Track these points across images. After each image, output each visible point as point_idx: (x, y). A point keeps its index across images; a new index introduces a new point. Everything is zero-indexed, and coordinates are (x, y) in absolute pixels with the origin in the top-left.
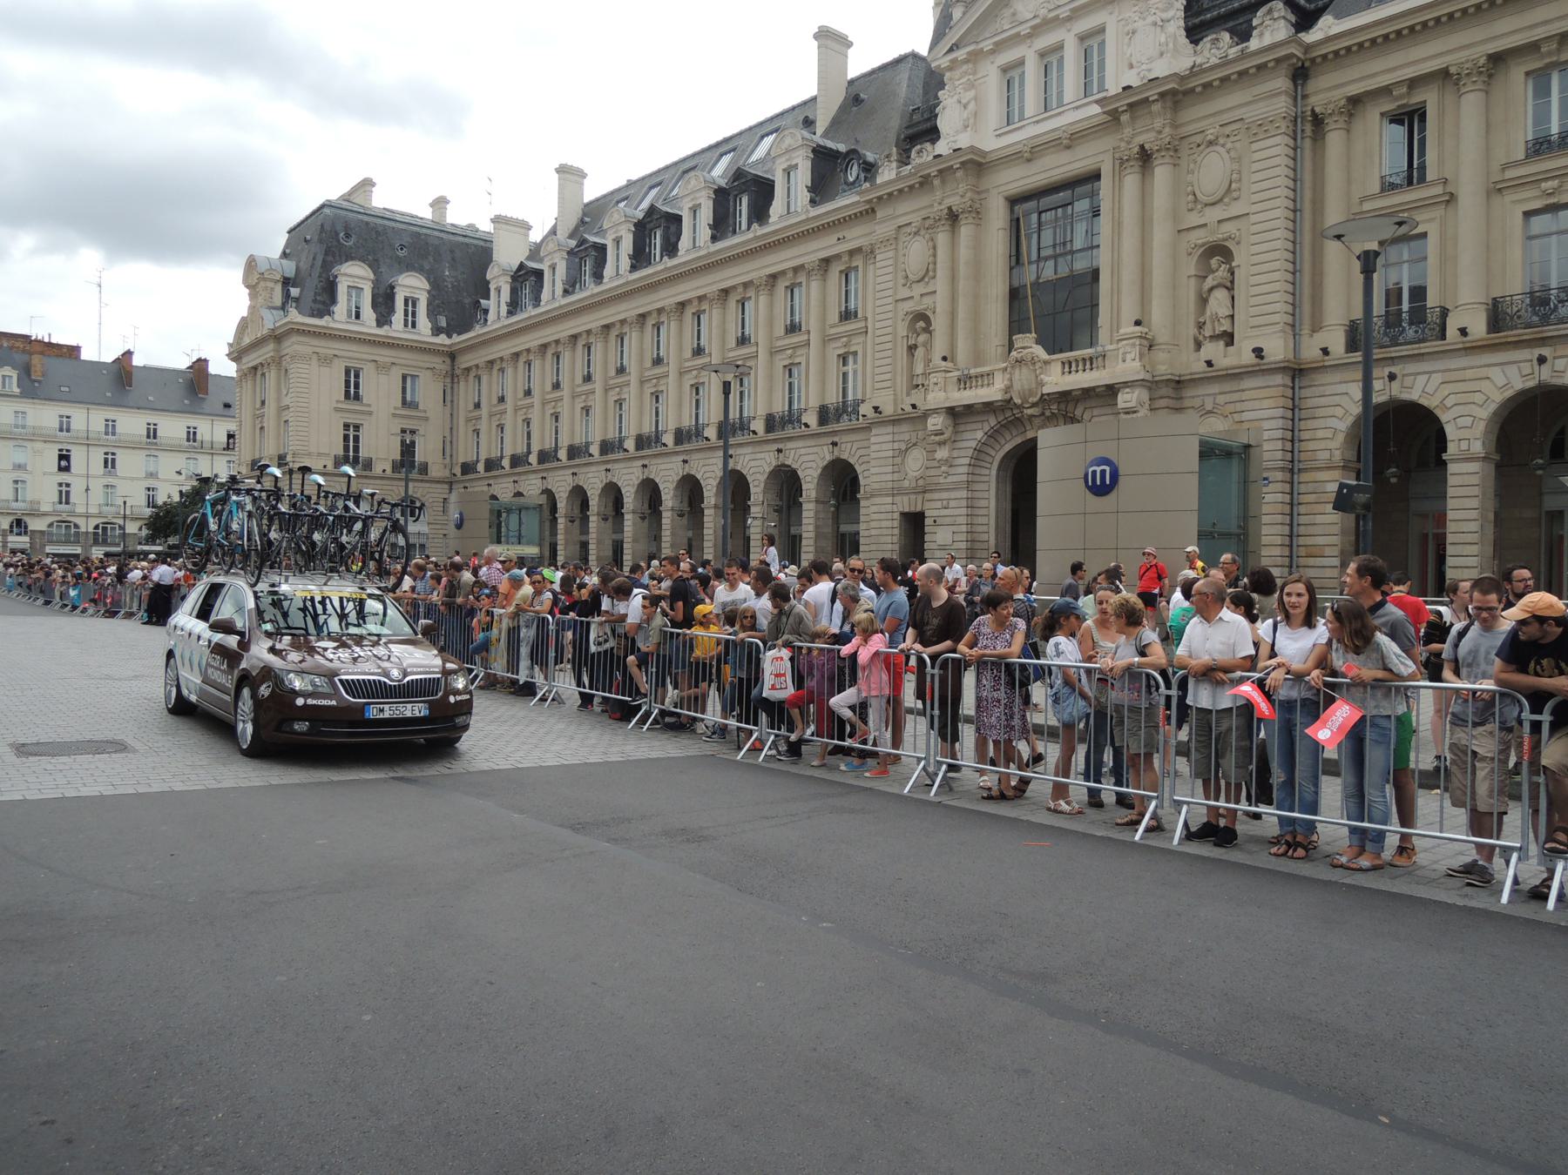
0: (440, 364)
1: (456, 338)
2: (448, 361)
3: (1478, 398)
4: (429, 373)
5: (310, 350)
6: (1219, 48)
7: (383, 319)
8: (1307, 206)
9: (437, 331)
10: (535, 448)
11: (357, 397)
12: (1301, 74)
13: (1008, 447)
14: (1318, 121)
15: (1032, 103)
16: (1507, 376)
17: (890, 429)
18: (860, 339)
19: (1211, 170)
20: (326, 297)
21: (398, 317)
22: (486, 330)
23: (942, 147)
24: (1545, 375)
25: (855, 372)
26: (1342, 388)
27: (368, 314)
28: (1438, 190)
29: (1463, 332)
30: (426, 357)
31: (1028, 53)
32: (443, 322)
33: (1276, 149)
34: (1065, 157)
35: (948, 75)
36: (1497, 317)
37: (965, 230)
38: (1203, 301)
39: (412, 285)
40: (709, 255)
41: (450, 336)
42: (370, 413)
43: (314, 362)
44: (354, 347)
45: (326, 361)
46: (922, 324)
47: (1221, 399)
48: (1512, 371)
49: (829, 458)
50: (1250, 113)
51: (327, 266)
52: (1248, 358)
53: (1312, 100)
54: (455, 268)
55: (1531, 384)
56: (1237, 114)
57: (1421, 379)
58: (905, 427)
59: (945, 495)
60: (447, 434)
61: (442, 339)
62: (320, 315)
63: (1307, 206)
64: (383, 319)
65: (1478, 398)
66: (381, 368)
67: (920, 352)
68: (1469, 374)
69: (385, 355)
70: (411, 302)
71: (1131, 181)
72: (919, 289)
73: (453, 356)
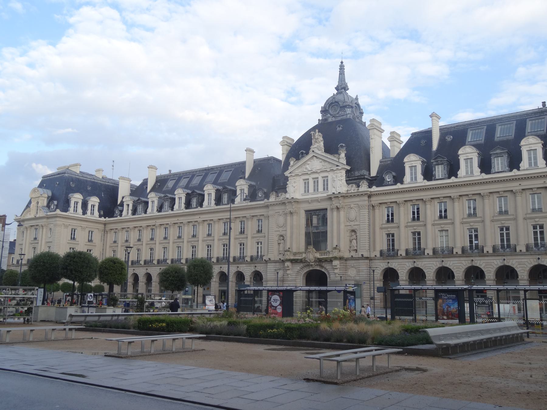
0: (101, 227)
1: (107, 219)
2: (103, 226)
3: (404, 268)
4: (97, 230)
5: (62, 223)
6: (353, 189)
7: (84, 213)
8: (371, 224)
9: (100, 216)
10: (131, 259)
11: (74, 239)
12: (370, 196)
13: (305, 271)
14: (373, 206)
15: (311, 189)
16: (530, 262)
17: (274, 264)
18: (263, 238)
19: (353, 214)
20: (65, 206)
21: (89, 212)
22: (121, 218)
23: (288, 196)
24: (416, 265)
25: (261, 247)
26: (379, 264)
27: (80, 210)
28: (396, 225)
29: (401, 255)
30: (97, 225)
31: (310, 178)
32: (102, 213)
33: (365, 212)
34: (319, 204)
35: (289, 178)
36: (435, 251)
37: (295, 217)
38: (351, 242)
39: (94, 201)
40: (215, 209)
41: (105, 218)
42: (78, 244)
43: (63, 227)
44: (75, 222)
45: (66, 226)
46: (282, 238)
47: (355, 264)
48: (467, 262)
49: (254, 270)
50: (360, 203)
51: (67, 194)
52: (360, 256)
53: (372, 202)
54: (108, 197)
55: (502, 264)
56: (357, 203)
57: (511, 261)
58: (277, 264)
59: (289, 282)
60: (102, 251)
61: (103, 219)
62: (66, 212)
63: (371, 224)
64: (84, 213)
65: (404, 268)
66: (83, 228)
67: (281, 245)
68: (402, 263)
69: (84, 224)
70: (93, 206)
71: (335, 213)
72: (281, 229)
73: (105, 224)
